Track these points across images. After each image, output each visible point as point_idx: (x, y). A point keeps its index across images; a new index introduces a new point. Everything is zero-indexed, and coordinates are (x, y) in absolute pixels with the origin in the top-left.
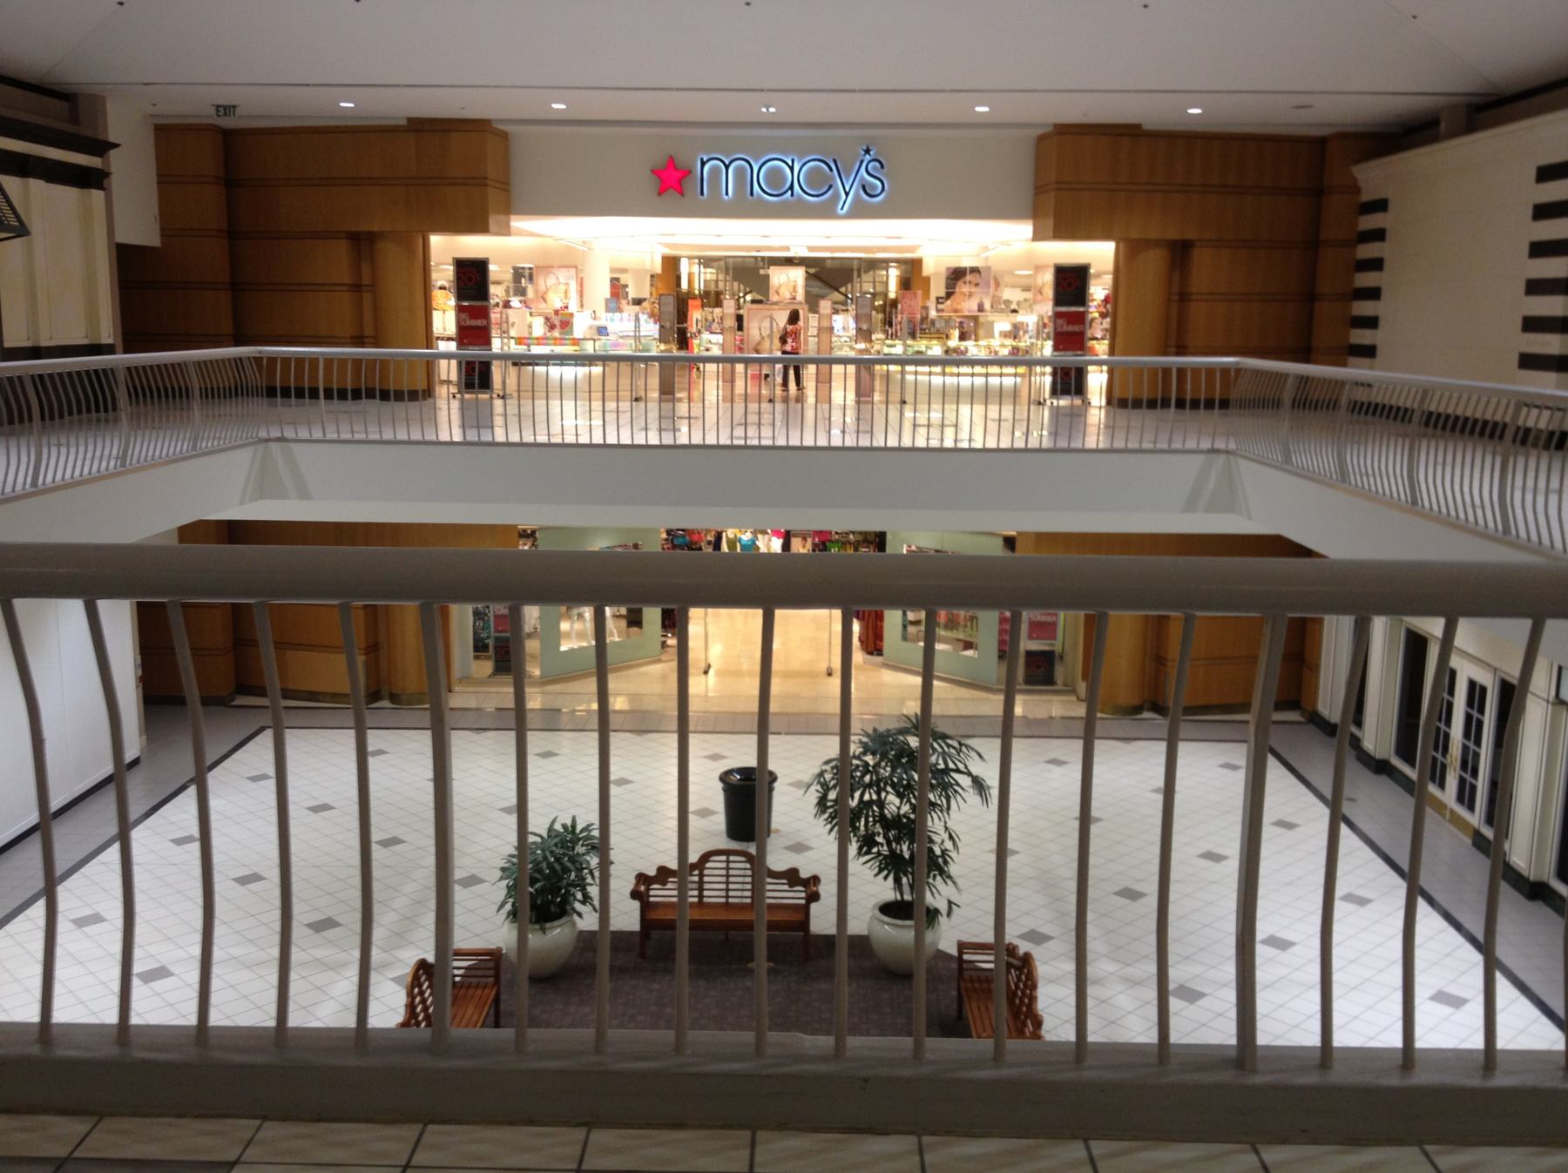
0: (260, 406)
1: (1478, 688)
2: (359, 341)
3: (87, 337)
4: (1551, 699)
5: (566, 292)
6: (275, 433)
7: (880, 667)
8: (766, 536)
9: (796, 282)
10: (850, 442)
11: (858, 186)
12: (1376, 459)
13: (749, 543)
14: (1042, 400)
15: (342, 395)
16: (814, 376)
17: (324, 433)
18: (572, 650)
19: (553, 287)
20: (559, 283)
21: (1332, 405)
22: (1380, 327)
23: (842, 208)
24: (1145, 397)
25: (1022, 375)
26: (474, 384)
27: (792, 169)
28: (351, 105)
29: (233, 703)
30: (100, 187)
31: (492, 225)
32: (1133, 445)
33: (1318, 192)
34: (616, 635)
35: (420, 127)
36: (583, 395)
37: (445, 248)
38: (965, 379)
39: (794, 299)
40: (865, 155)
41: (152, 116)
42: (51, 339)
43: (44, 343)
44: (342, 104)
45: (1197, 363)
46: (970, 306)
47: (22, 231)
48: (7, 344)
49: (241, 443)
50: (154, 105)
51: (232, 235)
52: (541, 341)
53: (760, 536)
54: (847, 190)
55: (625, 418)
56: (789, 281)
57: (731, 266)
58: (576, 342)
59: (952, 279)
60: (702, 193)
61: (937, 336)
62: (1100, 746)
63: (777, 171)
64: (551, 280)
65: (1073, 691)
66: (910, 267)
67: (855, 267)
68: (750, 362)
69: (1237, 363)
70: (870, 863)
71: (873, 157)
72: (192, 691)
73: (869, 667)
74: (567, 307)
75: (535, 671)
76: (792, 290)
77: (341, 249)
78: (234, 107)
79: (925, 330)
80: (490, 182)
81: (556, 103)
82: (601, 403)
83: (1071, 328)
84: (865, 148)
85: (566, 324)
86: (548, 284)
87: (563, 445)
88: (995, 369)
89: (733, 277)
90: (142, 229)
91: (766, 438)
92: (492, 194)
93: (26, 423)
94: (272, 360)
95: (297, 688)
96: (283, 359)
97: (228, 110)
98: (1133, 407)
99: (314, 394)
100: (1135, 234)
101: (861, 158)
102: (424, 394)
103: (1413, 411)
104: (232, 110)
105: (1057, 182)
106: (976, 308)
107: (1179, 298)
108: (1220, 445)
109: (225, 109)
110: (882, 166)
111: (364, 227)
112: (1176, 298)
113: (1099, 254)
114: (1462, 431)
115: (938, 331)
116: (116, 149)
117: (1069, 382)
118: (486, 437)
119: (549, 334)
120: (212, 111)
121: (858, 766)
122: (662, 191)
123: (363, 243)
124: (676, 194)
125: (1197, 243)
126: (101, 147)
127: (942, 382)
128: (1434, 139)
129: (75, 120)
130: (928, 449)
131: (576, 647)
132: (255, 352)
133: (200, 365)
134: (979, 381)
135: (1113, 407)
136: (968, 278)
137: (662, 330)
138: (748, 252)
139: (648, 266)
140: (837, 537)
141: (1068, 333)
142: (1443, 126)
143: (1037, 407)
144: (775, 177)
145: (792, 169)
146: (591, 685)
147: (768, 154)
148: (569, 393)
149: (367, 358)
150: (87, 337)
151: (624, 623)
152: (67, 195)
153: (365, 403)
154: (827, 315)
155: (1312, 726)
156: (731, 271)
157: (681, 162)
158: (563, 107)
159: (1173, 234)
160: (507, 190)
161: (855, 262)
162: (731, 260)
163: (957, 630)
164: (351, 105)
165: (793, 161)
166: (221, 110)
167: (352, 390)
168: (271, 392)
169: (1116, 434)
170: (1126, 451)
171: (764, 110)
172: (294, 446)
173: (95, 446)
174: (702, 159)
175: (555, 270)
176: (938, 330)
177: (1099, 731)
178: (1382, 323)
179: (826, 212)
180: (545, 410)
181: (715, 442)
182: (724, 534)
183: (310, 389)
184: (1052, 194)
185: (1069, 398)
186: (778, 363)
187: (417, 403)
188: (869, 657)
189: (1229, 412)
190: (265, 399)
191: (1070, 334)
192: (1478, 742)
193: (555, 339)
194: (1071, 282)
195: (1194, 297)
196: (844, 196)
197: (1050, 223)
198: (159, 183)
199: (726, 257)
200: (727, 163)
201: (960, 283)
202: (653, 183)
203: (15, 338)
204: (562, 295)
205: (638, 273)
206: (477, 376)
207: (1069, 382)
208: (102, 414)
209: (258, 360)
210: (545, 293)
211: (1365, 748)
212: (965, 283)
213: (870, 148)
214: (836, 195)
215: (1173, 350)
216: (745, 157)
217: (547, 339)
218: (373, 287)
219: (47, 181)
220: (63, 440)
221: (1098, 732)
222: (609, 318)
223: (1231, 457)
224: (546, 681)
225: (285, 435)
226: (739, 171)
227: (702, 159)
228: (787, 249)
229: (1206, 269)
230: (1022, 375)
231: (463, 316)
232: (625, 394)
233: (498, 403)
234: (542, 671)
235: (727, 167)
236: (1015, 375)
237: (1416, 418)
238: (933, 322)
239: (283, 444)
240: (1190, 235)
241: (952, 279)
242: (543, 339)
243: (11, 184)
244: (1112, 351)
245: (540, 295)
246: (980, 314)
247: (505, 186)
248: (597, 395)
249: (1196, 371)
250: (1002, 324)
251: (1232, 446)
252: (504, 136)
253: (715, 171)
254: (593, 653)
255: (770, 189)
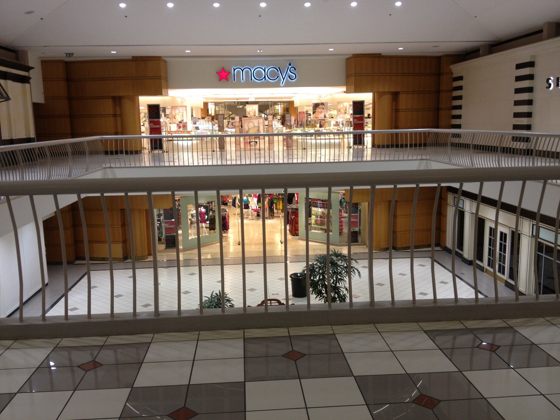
0: (102, 157)
1: (503, 234)
2: (116, 134)
3: (26, 135)
4: (530, 236)
5: (182, 115)
6: (108, 165)
7: (298, 240)
8: (251, 198)
9: (255, 110)
10: (286, 161)
11: (287, 76)
12: (463, 160)
13: (246, 200)
14: (306, 148)
15: (112, 153)
16: (268, 142)
17: (120, 165)
18: (192, 239)
19: (178, 113)
20: (180, 112)
21: (445, 145)
22: (462, 118)
23: (282, 84)
24: (386, 144)
25: (341, 139)
26: (157, 148)
27: (265, 71)
28: (115, 52)
29: (75, 263)
30: (29, 83)
31: (163, 93)
32: (382, 159)
33: (439, 75)
34: (207, 233)
35: (136, 59)
36: (190, 150)
37: (145, 101)
38: (322, 140)
39: (255, 116)
40: (289, 66)
41: (40, 57)
42: (16, 136)
43: (14, 138)
44: (112, 52)
45: (402, 131)
46: (321, 116)
47: (8, 99)
48: (3, 138)
49: (94, 170)
50: (44, 54)
51: (70, 98)
52: (176, 132)
53: (249, 198)
54: (284, 78)
55: (210, 157)
56: (253, 109)
57: (226, 105)
58: (189, 132)
59: (315, 107)
60: (234, 80)
61: (312, 126)
62: (375, 262)
63: (260, 72)
64: (177, 111)
65: (365, 244)
66: (288, 104)
67: (270, 104)
68: (270, 136)
69: (429, 130)
70: (321, 300)
71: (292, 66)
72: (64, 260)
73: (294, 240)
74: (183, 120)
75: (181, 247)
76: (254, 113)
77: (110, 102)
78: (73, 54)
79: (308, 124)
80: (162, 78)
81: (187, 50)
82: (197, 153)
83: (359, 122)
84: (289, 63)
85: (185, 126)
86: (176, 113)
87: (184, 166)
88: (332, 136)
89: (227, 109)
90: (40, 99)
91: (331, 160)
92: (163, 82)
93: (469, 149)
94: (106, 140)
95: (97, 256)
96: (110, 140)
97: (70, 55)
98: (387, 148)
99: (122, 152)
100: (381, 90)
101: (288, 67)
102: (138, 152)
103: (470, 144)
104: (72, 55)
105: (355, 73)
106: (323, 117)
107: (396, 111)
108: (424, 157)
109: (69, 55)
110: (295, 69)
111: (117, 94)
112: (394, 111)
113: (367, 97)
114: (491, 151)
115: (312, 125)
116: (33, 69)
117: (359, 140)
118: (162, 164)
119: (179, 130)
120: (65, 55)
121: (317, 267)
122: (220, 79)
123: (117, 100)
124: (225, 80)
125: (401, 93)
126: (28, 69)
127: (339, 141)
128: (478, 56)
129: (17, 58)
130: (311, 163)
131: (194, 238)
132: (100, 138)
133: (88, 142)
134: (327, 141)
135: (375, 148)
136: (320, 106)
137: (219, 127)
138: (267, 99)
139: (200, 106)
140: (275, 197)
141: (358, 124)
142: (481, 52)
143: (304, 150)
144: (259, 74)
145: (265, 71)
146: (196, 251)
147: (255, 67)
148: (185, 150)
149: (119, 138)
150: (26, 135)
151: (208, 229)
152: (18, 85)
153: (120, 156)
154: (271, 120)
155: (445, 251)
156: (226, 107)
157: (227, 69)
158: (189, 51)
159: (393, 90)
160: (167, 80)
161: (270, 103)
162: (226, 103)
163: (324, 226)
164: (115, 52)
165: (265, 68)
166: (68, 55)
167: (115, 151)
168: (106, 153)
169: (386, 156)
170: (380, 161)
171: (259, 51)
172: (114, 169)
173: (9, 176)
174: (234, 68)
175: (178, 108)
176: (312, 124)
177: (374, 256)
178: (463, 117)
179: (277, 85)
180: (335, 151)
181: (245, 163)
182: (237, 198)
183: (110, 151)
184: (353, 77)
185: (357, 145)
186: (218, 137)
187: (138, 155)
188: (293, 236)
189: (427, 148)
190: (104, 155)
191: (358, 124)
192: (505, 252)
193: (181, 131)
194: (358, 107)
195: (400, 110)
196: (282, 80)
197: (353, 87)
198: (43, 81)
199: (224, 102)
200: (243, 69)
201: (318, 108)
202: (217, 77)
203: (5, 136)
204: (181, 116)
205: (197, 108)
206: (157, 144)
207: (359, 140)
208: (33, 162)
209: (101, 140)
210: (175, 116)
211: (464, 257)
212: (319, 108)
213: (291, 63)
214: (280, 80)
215: (394, 128)
216: (240, 68)
217: (178, 131)
218: (121, 115)
219: (13, 81)
220: (33, 170)
221: (374, 257)
222: (199, 124)
223: (428, 161)
224: (185, 250)
225: (111, 166)
226: (247, 72)
227: (234, 68)
228: (248, 99)
229: (404, 101)
230: (341, 139)
231: (151, 124)
232: (209, 150)
233: (165, 154)
234: (183, 247)
235: (243, 71)
236: (339, 139)
237: (471, 146)
238: (310, 122)
239: (111, 169)
240: (399, 90)
241: (315, 107)
242: (177, 131)
243: (2, 82)
244: (373, 128)
245: (173, 116)
246: (325, 118)
247: (166, 79)
248: (200, 150)
249: (402, 134)
250: (333, 122)
251: (428, 158)
252: (165, 62)
253: (238, 72)
254: (197, 240)
255: (257, 78)
